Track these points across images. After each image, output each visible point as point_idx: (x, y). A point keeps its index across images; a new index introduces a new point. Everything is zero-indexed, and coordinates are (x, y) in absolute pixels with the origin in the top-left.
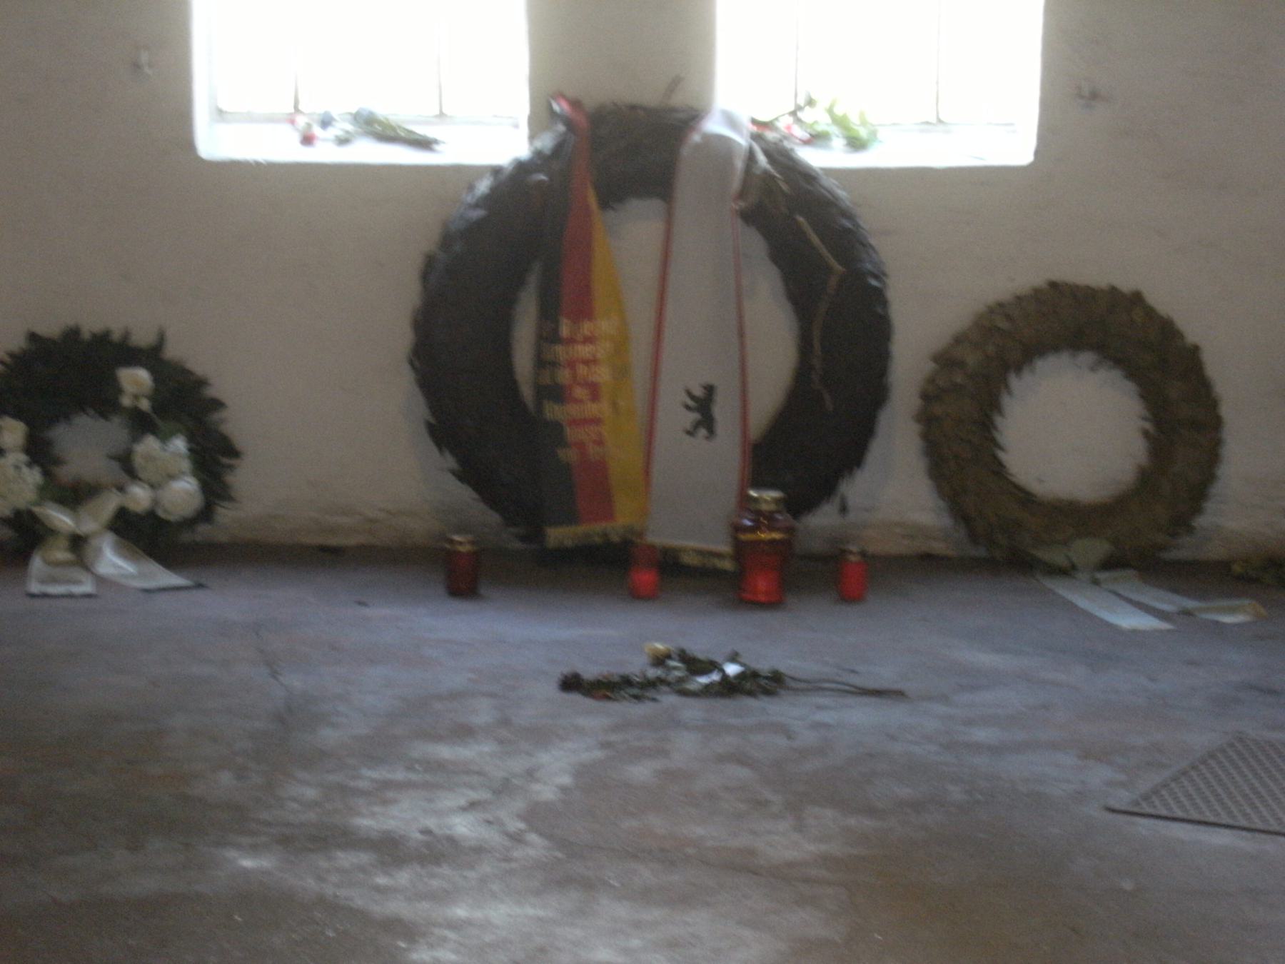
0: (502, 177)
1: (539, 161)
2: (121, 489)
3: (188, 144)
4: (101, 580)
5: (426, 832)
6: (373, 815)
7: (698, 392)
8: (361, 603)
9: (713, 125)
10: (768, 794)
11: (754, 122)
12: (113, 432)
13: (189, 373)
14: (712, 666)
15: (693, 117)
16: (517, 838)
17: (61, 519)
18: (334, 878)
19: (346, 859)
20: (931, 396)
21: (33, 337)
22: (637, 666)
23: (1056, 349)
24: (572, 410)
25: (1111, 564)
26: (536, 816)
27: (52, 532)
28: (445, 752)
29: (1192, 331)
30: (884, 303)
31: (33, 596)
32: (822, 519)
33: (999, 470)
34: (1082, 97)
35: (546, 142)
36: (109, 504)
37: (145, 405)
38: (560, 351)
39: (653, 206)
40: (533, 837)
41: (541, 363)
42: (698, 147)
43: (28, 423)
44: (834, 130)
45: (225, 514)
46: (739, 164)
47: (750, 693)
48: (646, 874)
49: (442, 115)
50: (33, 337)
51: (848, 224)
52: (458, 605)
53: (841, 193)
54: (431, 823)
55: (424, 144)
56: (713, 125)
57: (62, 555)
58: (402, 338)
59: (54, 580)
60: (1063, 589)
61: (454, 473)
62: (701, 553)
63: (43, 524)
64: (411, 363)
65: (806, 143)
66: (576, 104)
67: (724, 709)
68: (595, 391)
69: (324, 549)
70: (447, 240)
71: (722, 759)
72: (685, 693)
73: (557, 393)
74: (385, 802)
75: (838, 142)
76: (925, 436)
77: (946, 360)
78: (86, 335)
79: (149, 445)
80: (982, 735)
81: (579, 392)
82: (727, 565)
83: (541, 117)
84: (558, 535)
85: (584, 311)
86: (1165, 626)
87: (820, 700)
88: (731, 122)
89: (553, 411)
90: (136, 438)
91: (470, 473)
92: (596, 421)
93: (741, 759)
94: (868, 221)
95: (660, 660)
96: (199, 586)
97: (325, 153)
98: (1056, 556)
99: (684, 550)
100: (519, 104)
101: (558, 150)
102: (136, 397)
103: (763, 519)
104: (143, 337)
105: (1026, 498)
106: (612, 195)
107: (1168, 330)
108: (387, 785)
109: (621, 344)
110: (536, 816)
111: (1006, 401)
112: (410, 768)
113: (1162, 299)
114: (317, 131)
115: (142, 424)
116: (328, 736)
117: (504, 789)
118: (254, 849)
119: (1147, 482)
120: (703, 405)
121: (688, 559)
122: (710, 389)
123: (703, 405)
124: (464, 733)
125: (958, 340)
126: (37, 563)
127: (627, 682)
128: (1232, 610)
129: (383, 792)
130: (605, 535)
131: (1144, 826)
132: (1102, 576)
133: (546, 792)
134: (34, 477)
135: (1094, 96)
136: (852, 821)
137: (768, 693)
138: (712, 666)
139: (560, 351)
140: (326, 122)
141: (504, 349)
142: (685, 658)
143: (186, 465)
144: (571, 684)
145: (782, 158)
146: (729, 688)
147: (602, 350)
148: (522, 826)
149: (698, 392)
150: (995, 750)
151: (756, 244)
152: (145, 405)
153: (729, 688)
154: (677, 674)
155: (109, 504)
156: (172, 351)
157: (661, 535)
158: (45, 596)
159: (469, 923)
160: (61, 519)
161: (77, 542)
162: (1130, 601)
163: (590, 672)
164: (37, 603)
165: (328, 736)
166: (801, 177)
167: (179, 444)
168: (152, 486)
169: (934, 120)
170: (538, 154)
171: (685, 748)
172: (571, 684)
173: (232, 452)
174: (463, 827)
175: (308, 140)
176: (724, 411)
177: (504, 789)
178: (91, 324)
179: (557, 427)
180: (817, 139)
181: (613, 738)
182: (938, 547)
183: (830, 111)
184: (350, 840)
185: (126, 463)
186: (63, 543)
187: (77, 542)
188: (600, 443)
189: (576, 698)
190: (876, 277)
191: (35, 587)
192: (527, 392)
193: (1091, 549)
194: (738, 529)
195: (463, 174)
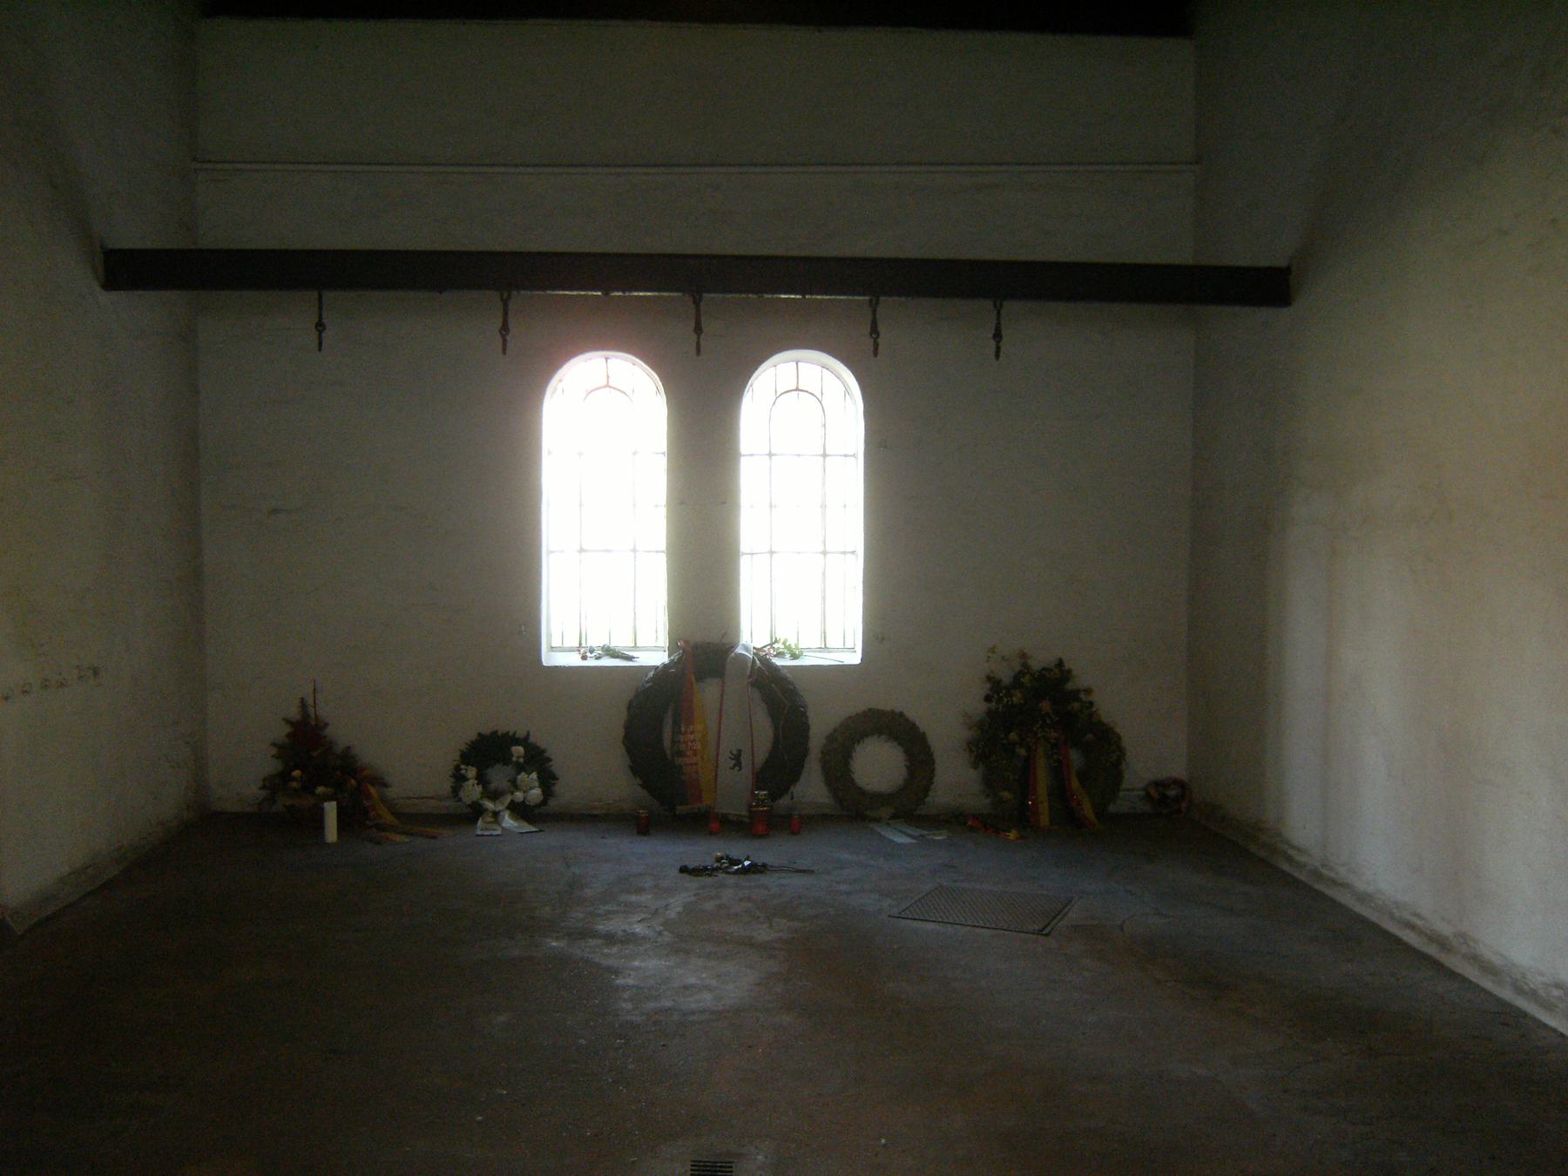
0: (658, 670)
2: (512, 793)
4: (503, 829)
5: (625, 931)
6: (604, 924)
7: (735, 753)
8: (603, 838)
9: (740, 650)
10: (758, 913)
11: (754, 648)
12: (509, 770)
13: (538, 748)
14: (738, 862)
15: (733, 646)
16: (660, 933)
17: (490, 805)
18: (588, 950)
19: (592, 942)
20: (825, 753)
21: (479, 734)
22: (710, 862)
23: (872, 734)
24: (687, 760)
25: (895, 817)
26: (667, 924)
27: (486, 810)
28: (633, 898)
29: (923, 726)
30: (807, 718)
31: (478, 835)
32: (784, 801)
34: (877, 638)
35: (675, 657)
36: (508, 799)
37: (521, 760)
38: (682, 738)
40: (666, 933)
41: (674, 742)
42: (733, 658)
43: (477, 768)
44: (786, 651)
45: (553, 803)
46: (750, 665)
47: (754, 873)
48: (709, 948)
49: (635, 646)
50: (479, 734)
51: (792, 687)
52: (643, 838)
53: (788, 675)
54: (627, 927)
55: (630, 658)
56: (740, 650)
58: (620, 732)
59: (487, 829)
60: (871, 825)
61: (640, 785)
62: (735, 815)
63: (1352, 911)
64: (624, 743)
65: (775, 656)
66: (686, 642)
67: (743, 880)
69: (589, 815)
70: (637, 695)
71: (741, 900)
72: (728, 873)
73: (680, 754)
74: (608, 919)
75: (788, 656)
76: (823, 768)
77: (831, 738)
78: (499, 734)
79: (523, 776)
80: (843, 887)
81: (688, 753)
82: (747, 820)
84: (680, 809)
86: (915, 841)
87: (784, 875)
88: (746, 648)
89: (679, 761)
90: (519, 773)
92: (696, 764)
93: (749, 899)
95: (719, 860)
96: (541, 831)
97: (591, 663)
99: (730, 814)
100: (664, 641)
101: (680, 659)
102: (518, 757)
103: (760, 802)
104: (521, 734)
105: (862, 792)
106: (700, 678)
107: (913, 726)
108: (609, 912)
110: (667, 924)
111: (854, 754)
112: (619, 905)
113: (911, 714)
114: (589, 654)
115: (520, 768)
116: (588, 892)
117: (656, 913)
118: (557, 939)
120: (737, 758)
121: (731, 817)
122: (740, 751)
123: (737, 758)
124: (640, 890)
125: (835, 731)
126: (480, 822)
127: (706, 868)
128: (940, 835)
129: (608, 915)
130: (699, 809)
131: (903, 923)
132: (891, 822)
133: (672, 914)
134: (479, 789)
135: (883, 639)
136: (790, 924)
137: (761, 872)
138: (738, 862)
139: (682, 738)
140: (591, 652)
142: (728, 858)
143: (537, 784)
144: (684, 870)
145: (765, 662)
146: (745, 871)
148: (662, 928)
149: (735, 753)
150: (849, 893)
151: (757, 695)
152: (521, 760)
153: (745, 871)
154: (725, 865)
155: (508, 799)
156: (532, 739)
157: (723, 808)
158: (483, 835)
159: (638, 968)
160: (490, 805)
161: (496, 814)
162: (900, 831)
163: (692, 865)
164: (480, 838)
165: (588, 892)
166: (776, 669)
167: (534, 775)
168: (524, 792)
169: (823, 646)
170: (671, 661)
171: (727, 894)
172: (684, 870)
173: (555, 778)
174: (638, 929)
175: (584, 658)
176: (745, 760)
177: (656, 913)
180: (780, 655)
181: (701, 892)
182: (828, 811)
183: (784, 643)
184: (594, 935)
185: (514, 782)
186: (490, 815)
187: (496, 814)
188: (697, 773)
189: (685, 875)
190: (803, 707)
191: (479, 832)
193: (885, 812)
194: (751, 806)
195: (644, 669)
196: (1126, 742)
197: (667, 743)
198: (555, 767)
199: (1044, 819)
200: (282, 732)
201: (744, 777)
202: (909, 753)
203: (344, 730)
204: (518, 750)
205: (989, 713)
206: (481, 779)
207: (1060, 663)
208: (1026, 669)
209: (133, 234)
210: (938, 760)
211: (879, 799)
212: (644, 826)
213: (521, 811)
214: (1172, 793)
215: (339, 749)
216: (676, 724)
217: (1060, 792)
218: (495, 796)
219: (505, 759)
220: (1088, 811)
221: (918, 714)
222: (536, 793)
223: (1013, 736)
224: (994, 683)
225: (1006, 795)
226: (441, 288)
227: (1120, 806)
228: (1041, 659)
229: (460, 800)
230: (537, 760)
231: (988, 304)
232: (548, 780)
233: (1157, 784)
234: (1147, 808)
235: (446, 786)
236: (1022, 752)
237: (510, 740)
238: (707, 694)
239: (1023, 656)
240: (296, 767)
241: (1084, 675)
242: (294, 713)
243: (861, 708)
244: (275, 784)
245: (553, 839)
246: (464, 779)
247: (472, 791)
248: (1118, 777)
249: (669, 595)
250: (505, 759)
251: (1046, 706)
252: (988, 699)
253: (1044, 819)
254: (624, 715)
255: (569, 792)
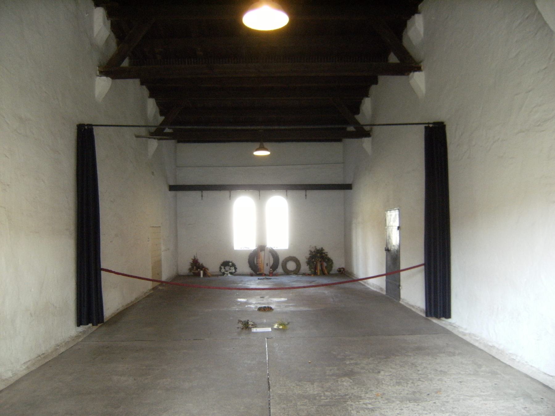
1: (256, 249)
3: (234, 249)
9: (267, 246)
12: (229, 267)
20: (282, 263)
22: (263, 278)
27: (225, 273)
33: (287, 268)
35: (257, 248)
39: (264, 252)
41: (257, 262)
56: (267, 246)
57: (226, 275)
58: (247, 261)
60: (291, 276)
68: (260, 264)
73: (257, 264)
77: (283, 261)
79: (231, 268)
83: (256, 246)
84: (258, 273)
85: (259, 258)
89: (258, 265)
91: (252, 269)
94: (277, 252)
98: (290, 274)
104: (231, 261)
105: (288, 270)
106: (261, 251)
109: (262, 260)
115: (231, 266)
119: (297, 268)
123: (267, 264)
141: (254, 261)
144: (306, 199)
147: (260, 261)
156: (233, 262)
160: (226, 272)
161: (227, 274)
167: (233, 268)
178: (228, 260)
179: (257, 266)
187: (227, 274)
192: (256, 264)
193: (292, 273)
196: (334, 262)
197: (255, 262)
198: (237, 267)
199: (319, 274)
200: (191, 261)
201: (269, 267)
202: (297, 264)
203: (201, 261)
204: (230, 264)
205: (310, 257)
206: (224, 268)
207: (322, 248)
208: (316, 249)
209: (172, 183)
210: (301, 264)
211: (291, 271)
212: (251, 275)
213: (231, 273)
214: (342, 270)
215: (201, 264)
216: (257, 259)
217: (322, 270)
218: (227, 271)
219: (229, 265)
220: (326, 272)
221: (299, 258)
222: (234, 271)
223: (313, 260)
224: (311, 251)
225: (312, 270)
226: (220, 190)
227: (332, 272)
228: (319, 247)
229: (221, 272)
230: (233, 265)
231: (305, 191)
232: (235, 269)
233: (339, 269)
234: (338, 273)
235: (218, 270)
236: (315, 263)
237: (228, 262)
238: (262, 254)
239: (315, 247)
240: (195, 266)
241: (326, 250)
242: (193, 258)
243: (289, 256)
244: (190, 270)
245: (236, 277)
246: (222, 268)
247: (223, 270)
248: (332, 267)
249: (256, 30)
250: (229, 265)
251: (319, 255)
252: (310, 254)
253: (319, 274)
254: (248, 258)
255: (238, 271)
